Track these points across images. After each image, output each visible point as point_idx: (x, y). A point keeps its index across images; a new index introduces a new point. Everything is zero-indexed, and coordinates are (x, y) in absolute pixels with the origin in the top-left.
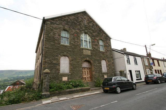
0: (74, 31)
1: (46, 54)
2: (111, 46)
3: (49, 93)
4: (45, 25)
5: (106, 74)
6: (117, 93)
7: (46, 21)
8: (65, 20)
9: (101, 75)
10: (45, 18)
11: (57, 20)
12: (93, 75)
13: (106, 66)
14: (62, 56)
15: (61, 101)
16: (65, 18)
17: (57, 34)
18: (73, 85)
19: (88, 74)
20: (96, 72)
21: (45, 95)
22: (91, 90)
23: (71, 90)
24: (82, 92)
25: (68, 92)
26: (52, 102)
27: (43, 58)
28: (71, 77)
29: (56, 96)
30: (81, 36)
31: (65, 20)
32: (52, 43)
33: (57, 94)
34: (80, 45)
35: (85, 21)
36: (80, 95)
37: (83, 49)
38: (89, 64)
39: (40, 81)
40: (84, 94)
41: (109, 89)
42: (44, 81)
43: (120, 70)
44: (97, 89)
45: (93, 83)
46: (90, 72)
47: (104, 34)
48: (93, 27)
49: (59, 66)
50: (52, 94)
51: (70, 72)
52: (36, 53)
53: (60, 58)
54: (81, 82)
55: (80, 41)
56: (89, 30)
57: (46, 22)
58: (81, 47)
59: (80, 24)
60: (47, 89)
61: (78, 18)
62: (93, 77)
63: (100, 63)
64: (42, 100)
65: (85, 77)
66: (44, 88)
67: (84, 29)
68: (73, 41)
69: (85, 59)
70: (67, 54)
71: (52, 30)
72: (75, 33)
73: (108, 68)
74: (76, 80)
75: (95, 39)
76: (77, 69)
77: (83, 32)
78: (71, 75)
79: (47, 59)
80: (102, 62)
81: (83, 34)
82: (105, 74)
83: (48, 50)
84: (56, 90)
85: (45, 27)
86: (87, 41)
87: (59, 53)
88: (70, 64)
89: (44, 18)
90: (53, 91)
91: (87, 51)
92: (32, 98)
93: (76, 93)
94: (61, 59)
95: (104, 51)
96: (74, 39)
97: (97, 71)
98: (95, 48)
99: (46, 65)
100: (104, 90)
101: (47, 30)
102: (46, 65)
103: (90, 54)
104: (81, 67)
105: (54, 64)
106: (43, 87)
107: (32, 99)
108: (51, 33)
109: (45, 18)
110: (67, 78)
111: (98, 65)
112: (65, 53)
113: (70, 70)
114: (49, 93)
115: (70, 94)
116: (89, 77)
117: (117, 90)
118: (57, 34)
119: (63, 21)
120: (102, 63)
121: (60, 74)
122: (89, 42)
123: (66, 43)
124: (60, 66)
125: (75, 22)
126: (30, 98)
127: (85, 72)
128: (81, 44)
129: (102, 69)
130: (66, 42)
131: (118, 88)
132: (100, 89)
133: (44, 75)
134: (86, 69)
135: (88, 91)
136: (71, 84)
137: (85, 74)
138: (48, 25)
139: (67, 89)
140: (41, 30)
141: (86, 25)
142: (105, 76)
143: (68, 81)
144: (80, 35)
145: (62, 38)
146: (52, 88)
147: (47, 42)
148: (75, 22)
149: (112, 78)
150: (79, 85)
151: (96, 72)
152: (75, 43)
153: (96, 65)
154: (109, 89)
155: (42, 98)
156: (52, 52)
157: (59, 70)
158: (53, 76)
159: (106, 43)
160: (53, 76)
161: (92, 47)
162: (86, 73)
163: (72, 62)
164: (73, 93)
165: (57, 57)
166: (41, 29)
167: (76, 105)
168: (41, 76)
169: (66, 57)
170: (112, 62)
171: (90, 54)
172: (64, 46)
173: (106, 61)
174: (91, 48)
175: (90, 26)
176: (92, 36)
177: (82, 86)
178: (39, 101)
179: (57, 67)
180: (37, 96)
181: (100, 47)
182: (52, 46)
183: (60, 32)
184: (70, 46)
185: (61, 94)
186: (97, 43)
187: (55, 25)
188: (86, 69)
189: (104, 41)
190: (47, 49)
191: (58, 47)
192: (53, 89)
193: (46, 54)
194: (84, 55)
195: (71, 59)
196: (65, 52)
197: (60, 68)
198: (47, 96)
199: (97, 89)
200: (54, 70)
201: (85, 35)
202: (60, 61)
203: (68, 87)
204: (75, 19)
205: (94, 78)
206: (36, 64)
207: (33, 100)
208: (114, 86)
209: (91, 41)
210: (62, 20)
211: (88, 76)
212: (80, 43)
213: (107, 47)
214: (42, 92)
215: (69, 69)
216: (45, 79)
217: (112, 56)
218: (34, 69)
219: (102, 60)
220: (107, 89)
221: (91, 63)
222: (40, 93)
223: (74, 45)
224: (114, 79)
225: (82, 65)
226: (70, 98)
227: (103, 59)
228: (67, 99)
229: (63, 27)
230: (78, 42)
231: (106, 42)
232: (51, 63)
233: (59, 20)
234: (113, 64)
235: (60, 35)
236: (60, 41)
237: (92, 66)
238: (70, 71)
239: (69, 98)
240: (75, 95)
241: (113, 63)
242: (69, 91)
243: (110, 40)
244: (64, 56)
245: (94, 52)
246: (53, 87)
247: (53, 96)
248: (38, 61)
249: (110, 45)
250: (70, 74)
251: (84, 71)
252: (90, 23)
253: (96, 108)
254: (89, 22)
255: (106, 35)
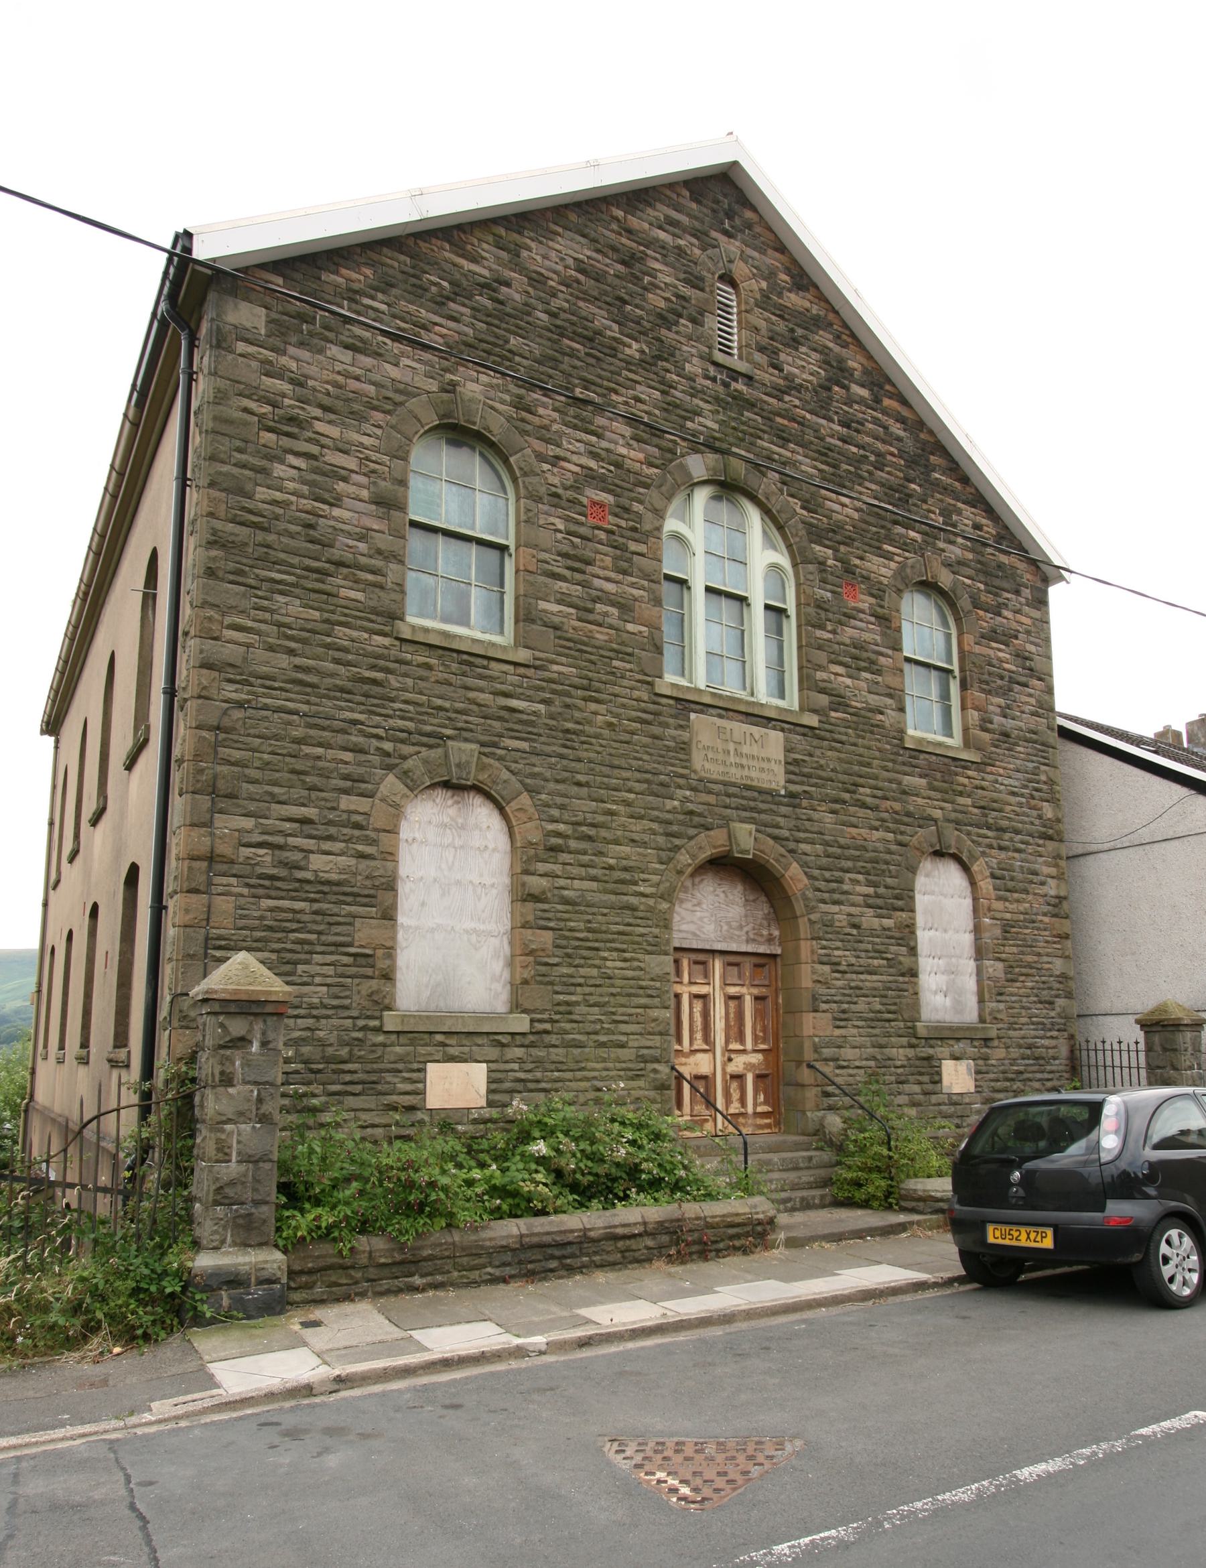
0: (574, 446)
1: (224, 752)
2: (1045, 677)
3: (279, 1256)
4: (192, 347)
5: (971, 1050)
6: (1160, 1300)
7: (212, 296)
8: (459, 292)
9: (900, 1054)
10: (201, 252)
11: (361, 276)
12: (809, 1055)
13: (967, 939)
14: (414, 787)
15: (447, 1364)
16: (467, 265)
17: (356, 489)
18: (559, 1174)
19: (736, 1031)
20: (841, 1019)
21: (234, 1281)
22: (792, 1243)
23: (540, 1225)
24: (681, 1258)
25: (505, 1248)
26: (339, 1380)
27: (178, 803)
28: (538, 1062)
29: (362, 1295)
30: (671, 524)
31: (459, 292)
32: (292, 608)
33: (372, 1272)
34: (659, 650)
35: (725, 308)
36: (671, 1296)
37: (686, 704)
38: (762, 909)
39: (145, 1111)
40: (709, 1290)
41: (1048, 1243)
42: (211, 1104)
43: (1145, 1003)
44: (859, 1234)
45: (797, 1147)
46: (759, 1014)
47: (968, 516)
48: (823, 408)
49: (389, 916)
50: (310, 1272)
51: (516, 1006)
52: (50, 740)
53: (397, 812)
54: (657, 1137)
55: (658, 602)
56: (783, 438)
57: (209, 313)
58: (670, 678)
59: (665, 353)
60: (257, 1203)
61: (629, 260)
62: (806, 1075)
63: (903, 900)
64: (206, 1342)
65: (705, 1069)
66: (221, 1197)
67: (708, 423)
68: (563, 586)
69: (709, 844)
70: (482, 767)
71: (292, 420)
72: (590, 477)
73: (995, 968)
74: (597, 1101)
75: (849, 570)
76: (613, 964)
77: (698, 466)
78: (535, 1038)
79: (229, 824)
80: (921, 882)
81: (701, 497)
82: (958, 1047)
83: (240, 705)
84: (364, 1226)
85: (190, 379)
86: (742, 600)
87: (388, 746)
88: (523, 896)
89: (188, 250)
90: (326, 1235)
91: (739, 728)
92: (76, 1308)
93: (601, 1266)
94: (405, 832)
95: (956, 741)
96: (578, 563)
97: (862, 1005)
98: (839, 702)
99: (224, 905)
100: (965, 1256)
101: (229, 422)
102: (224, 905)
103: (775, 778)
104: (656, 947)
105: (326, 887)
106: (202, 1184)
107: (75, 1325)
108: (279, 470)
109: (201, 252)
110: (477, 1074)
111: (870, 920)
112: (464, 751)
113: (525, 982)
114: (273, 1260)
115: (531, 1276)
116: (750, 1078)
117: (1166, 1260)
118: (356, 489)
119: (440, 303)
120: (922, 901)
121: (391, 1022)
122: (775, 612)
123: (474, 615)
124: (401, 919)
125: (602, 320)
126: (45, 1308)
127: (706, 1014)
128: (668, 632)
129: (913, 973)
130: (477, 599)
131: (1174, 1233)
132: (903, 1227)
133: (211, 1030)
134: (718, 965)
135: (745, 1251)
136: (541, 1160)
137: (707, 1038)
138: (241, 347)
139: (498, 1215)
140: (135, 425)
141: (734, 374)
142: (948, 1067)
143: (494, 1113)
144: (660, 514)
145: (416, 541)
146: (317, 1202)
147: (230, 592)
148: (602, 320)
149: (1096, 1109)
150: (633, 1171)
151: (841, 1019)
152: (584, 612)
153: (841, 920)
154: (1048, 1243)
155: (199, 1321)
156: (298, 733)
157: (388, 976)
158: (306, 1050)
159: (992, 636)
160: (306, 1050)
161: (805, 681)
162: (719, 1025)
163: (542, 867)
164: (571, 1270)
165: (362, 804)
166: (140, 405)
167: (670, 1442)
168: (163, 1038)
169: (477, 800)
170: (1052, 888)
171: (775, 778)
172: (445, 650)
173: (973, 883)
174: (792, 701)
175: (791, 386)
176: (816, 534)
177: (677, 1186)
178: (168, 1352)
179: (365, 933)
180: (136, 1291)
181: (916, 686)
182: (291, 652)
183: (402, 455)
184: (523, 655)
185: (417, 1280)
186: (871, 634)
187: (334, 351)
188: (718, 965)
189: (965, 603)
190: (231, 692)
191: (377, 660)
192: (328, 1219)
193: (224, 752)
194: (702, 785)
195: (532, 831)
196: (463, 733)
197: (390, 951)
198: (256, 1292)
199: (859, 1234)
200: (320, 965)
201: (724, 507)
202: (390, 856)
203: (494, 1191)
204: (599, 277)
205: (811, 1094)
206: (53, 884)
207: (85, 1339)
208: (1119, 1210)
209: (791, 606)
210: (418, 292)
211: (738, 1064)
212: (655, 627)
213: (1005, 692)
214: (196, 1245)
215: (511, 964)
216: (227, 1080)
217: (1048, 811)
218: (32, 943)
219: (927, 865)
220: (1023, 1242)
221: (787, 899)
222: (162, 1249)
223: (576, 648)
224: (1128, 1115)
225: (671, 910)
226: (557, 1336)
227: (939, 854)
228: (519, 1352)
229: (433, 386)
230: (625, 607)
231: (987, 621)
232: (283, 873)
233: (385, 285)
234: (1065, 926)
235: (402, 508)
236: (400, 588)
237: (790, 936)
238: (518, 987)
239: (539, 1340)
240: (607, 1296)
241: (1059, 906)
242: (524, 1248)
243: (1041, 602)
244: (447, 785)
245: (829, 758)
246: (268, 1148)
247: (320, 1302)
248: (98, 840)
249: (1037, 663)
250: (521, 1023)
251: (685, 991)
252: (794, 343)
253: (963, 1495)
254: (781, 327)
255: (990, 529)
